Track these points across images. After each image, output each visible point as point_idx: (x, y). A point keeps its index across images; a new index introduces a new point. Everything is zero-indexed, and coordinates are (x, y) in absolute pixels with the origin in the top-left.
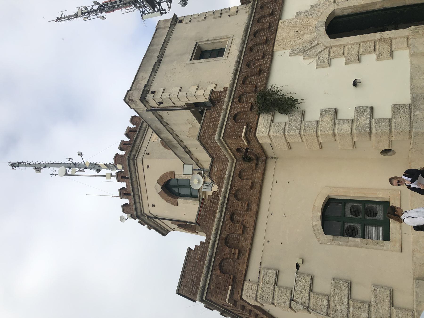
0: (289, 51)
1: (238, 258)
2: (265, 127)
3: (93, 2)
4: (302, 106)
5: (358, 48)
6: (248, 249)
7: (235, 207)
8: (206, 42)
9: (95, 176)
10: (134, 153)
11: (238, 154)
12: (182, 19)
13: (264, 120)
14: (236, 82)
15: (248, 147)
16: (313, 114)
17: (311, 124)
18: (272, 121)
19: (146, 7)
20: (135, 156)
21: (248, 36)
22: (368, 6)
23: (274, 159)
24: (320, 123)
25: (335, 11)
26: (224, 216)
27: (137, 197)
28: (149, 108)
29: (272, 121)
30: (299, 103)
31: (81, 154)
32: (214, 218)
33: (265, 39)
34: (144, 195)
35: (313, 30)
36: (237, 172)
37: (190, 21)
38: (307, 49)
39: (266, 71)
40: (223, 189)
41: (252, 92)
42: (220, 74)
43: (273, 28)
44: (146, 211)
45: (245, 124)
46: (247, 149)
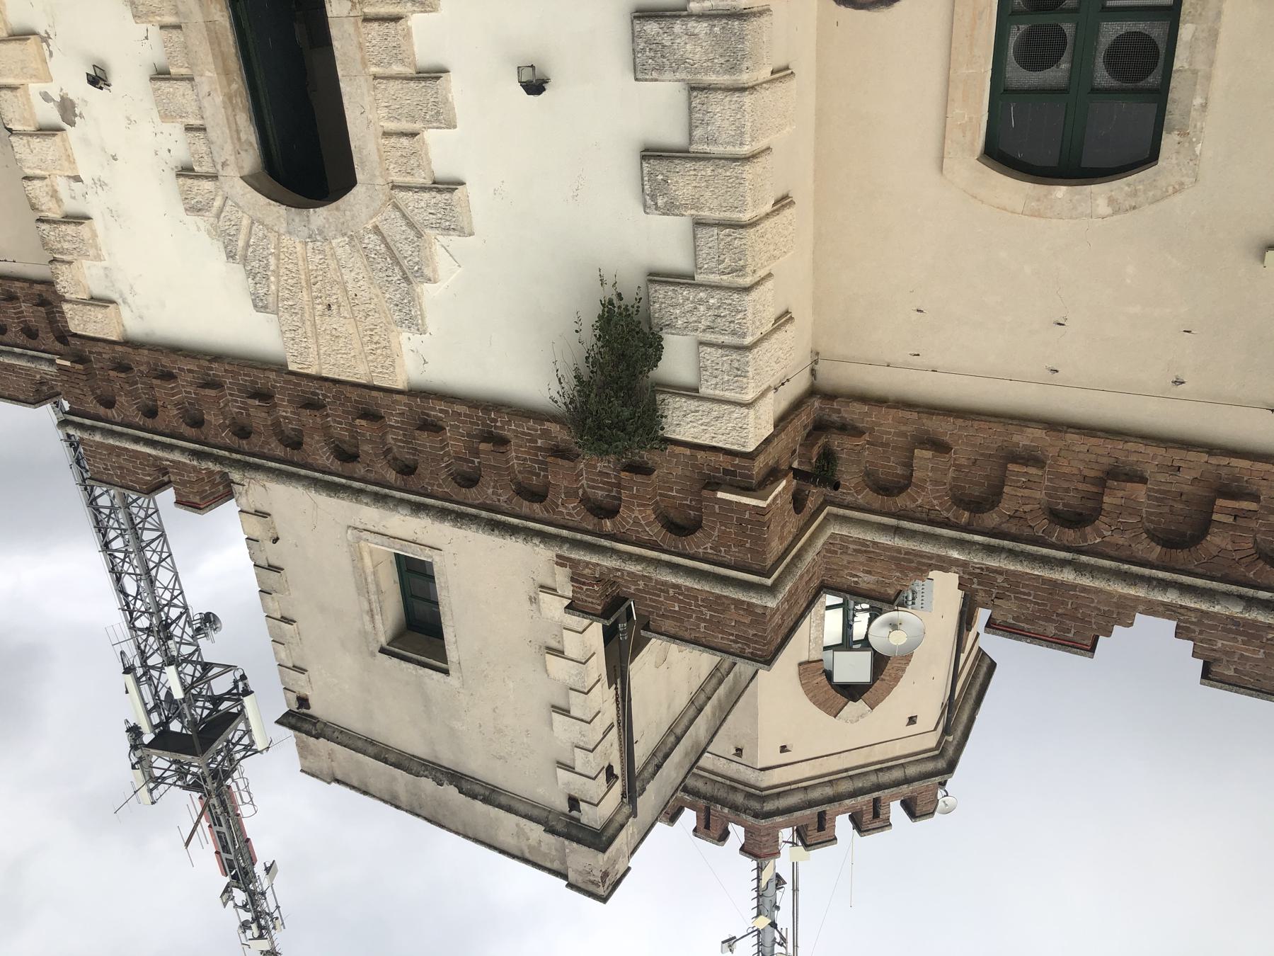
0: (405, 335)
1: (1255, 497)
2: (717, 418)
3: (225, 904)
4: (631, 284)
5: (392, 83)
6: (1214, 460)
7: (1027, 508)
8: (378, 618)
9: (795, 890)
10: (739, 799)
11: (810, 505)
12: (293, 697)
13: (686, 423)
14: (538, 526)
15: (791, 475)
16: (665, 240)
17: (706, 250)
18: (691, 392)
19: (229, 741)
20: (749, 796)
21: (356, 484)
22: (222, 53)
23: (817, 367)
24: (705, 213)
25: (246, 171)
26: (1068, 549)
27: (885, 778)
28: (626, 810)
29: (691, 392)
30: (619, 296)
31: (730, 942)
32: (1074, 587)
33: (363, 422)
34: (878, 754)
35: (321, 252)
36: (877, 501)
37: (302, 670)
38: (397, 269)
39: (489, 417)
40: (955, 554)
41: (575, 468)
42: (497, 580)
43: (316, 393)
44: (931, 741)
45: (706, 493)
46: (798, 474)
